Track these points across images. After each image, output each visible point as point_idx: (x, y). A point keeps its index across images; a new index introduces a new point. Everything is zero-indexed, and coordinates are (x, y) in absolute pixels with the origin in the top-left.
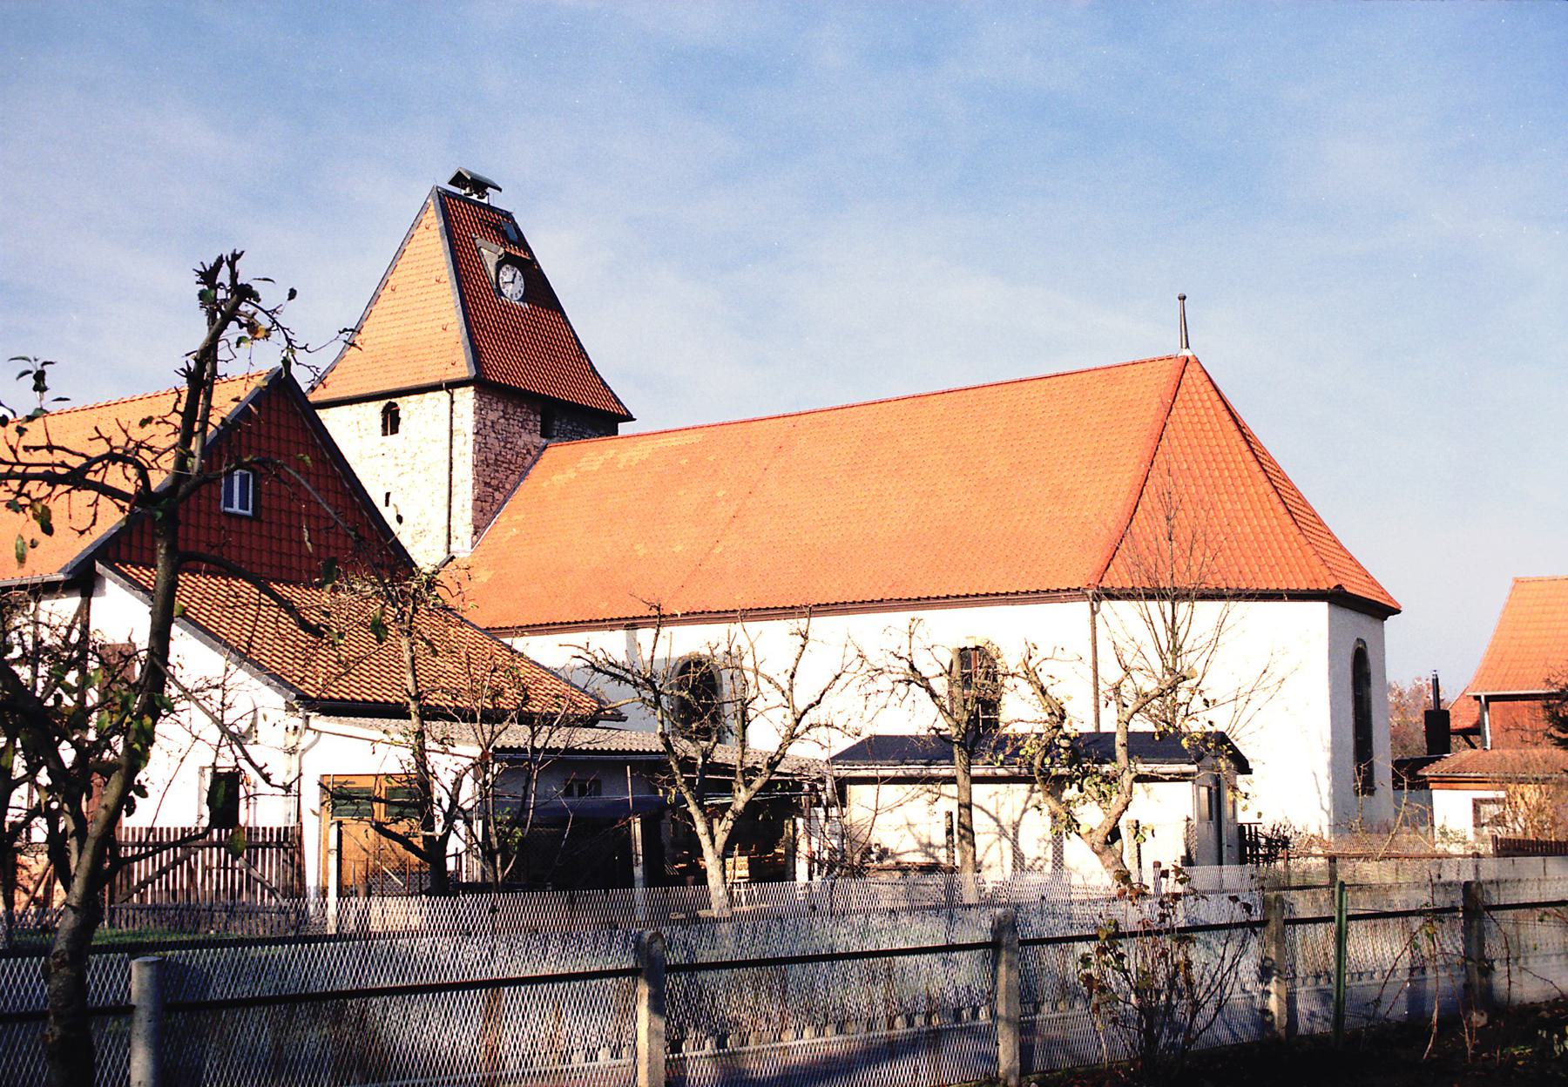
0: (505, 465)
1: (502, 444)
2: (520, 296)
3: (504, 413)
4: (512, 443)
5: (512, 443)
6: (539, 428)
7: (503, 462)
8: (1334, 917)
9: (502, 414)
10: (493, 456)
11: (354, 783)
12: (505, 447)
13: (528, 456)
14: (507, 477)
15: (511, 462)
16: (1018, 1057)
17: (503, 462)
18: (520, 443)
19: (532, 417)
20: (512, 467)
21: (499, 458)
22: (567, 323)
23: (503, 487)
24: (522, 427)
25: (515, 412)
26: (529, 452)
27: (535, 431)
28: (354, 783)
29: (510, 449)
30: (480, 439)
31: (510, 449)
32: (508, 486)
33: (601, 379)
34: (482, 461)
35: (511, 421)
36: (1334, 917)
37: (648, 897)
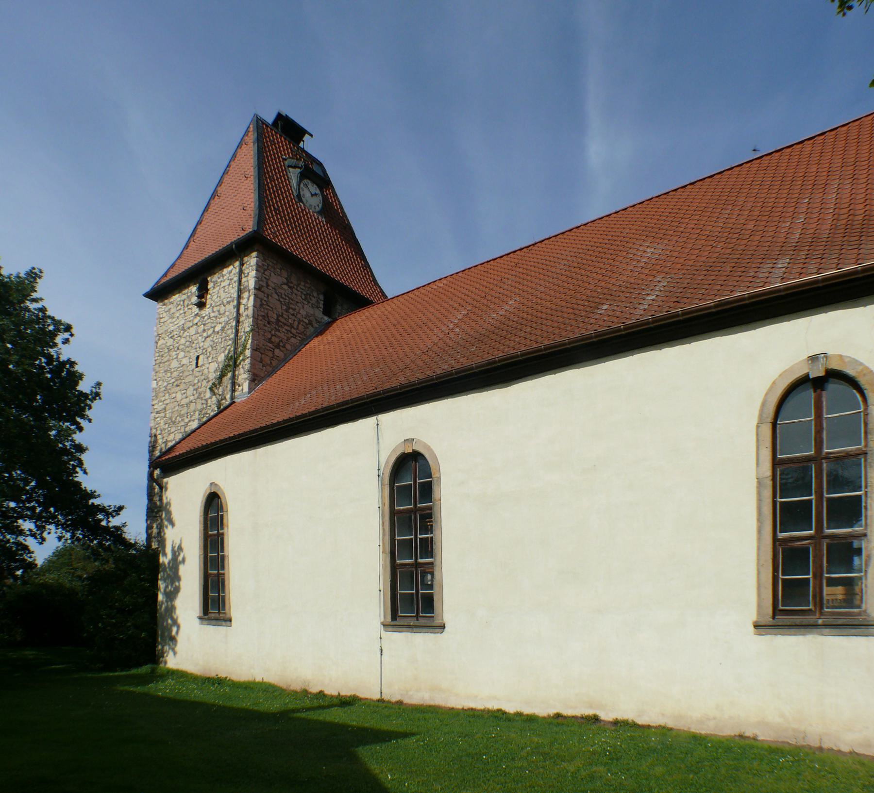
0: (286, 327)
1: (284, 307)
2: (318, 209)
3: (288, 281)
4: (294, 310)
5: (294, 310)
6: (321, 306)
7: (285, 324)
8: (828, 585)
9: (285, 281)
10: (275, 316)
11: (68, 569)
12: (287, 311)
13: (310, 327)
14: (288, 339)
15: (293, 327)
16: (360, 395)
17: (285, 324)
18: (303, 312)
19: (315, 294)
20: (294, 331)
21: (280, 318)
22: (367, 266)
23: (284, 347)
24: (305, 300)
25: (298, 285)
26: (310, 323)
27: (318, 307)
28: (68, 569)
29: (293, 315)
30: (261, 295)
31: (293, 315)
32: (288, 347)
33: (381, 289)
34: (263, 316)
35: (295, 291)
36: (828, 585)
37: (827, 466)
